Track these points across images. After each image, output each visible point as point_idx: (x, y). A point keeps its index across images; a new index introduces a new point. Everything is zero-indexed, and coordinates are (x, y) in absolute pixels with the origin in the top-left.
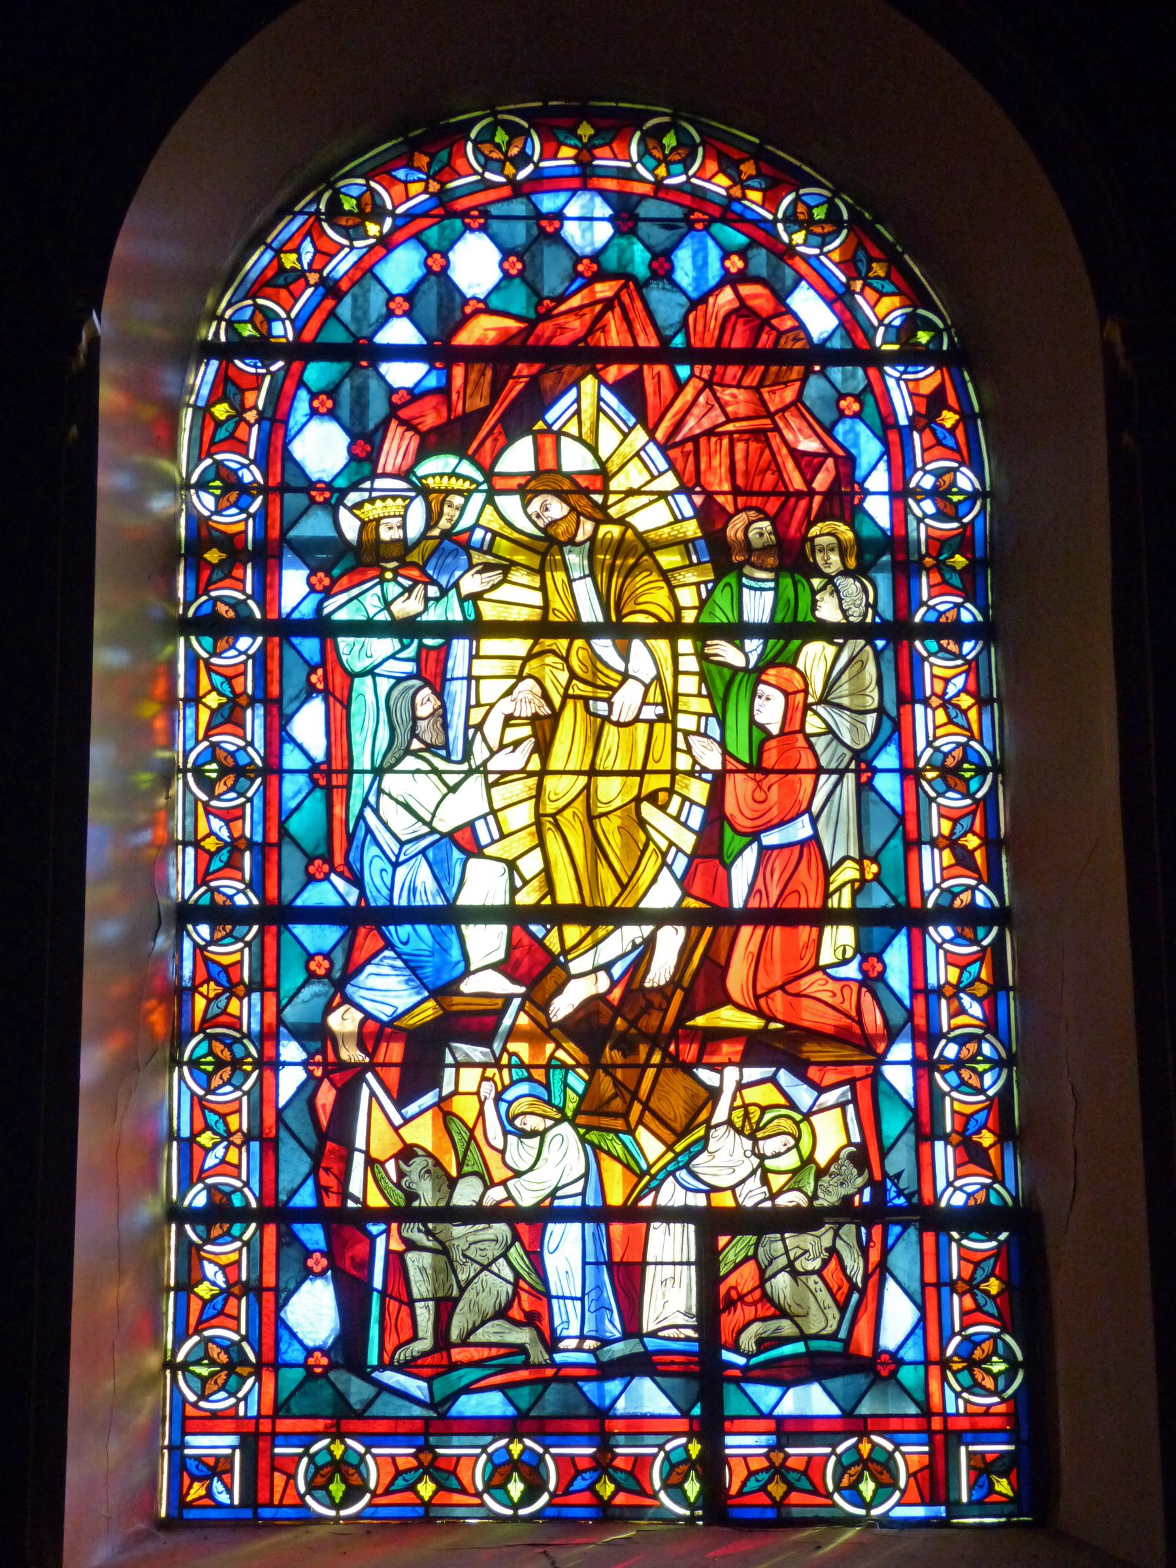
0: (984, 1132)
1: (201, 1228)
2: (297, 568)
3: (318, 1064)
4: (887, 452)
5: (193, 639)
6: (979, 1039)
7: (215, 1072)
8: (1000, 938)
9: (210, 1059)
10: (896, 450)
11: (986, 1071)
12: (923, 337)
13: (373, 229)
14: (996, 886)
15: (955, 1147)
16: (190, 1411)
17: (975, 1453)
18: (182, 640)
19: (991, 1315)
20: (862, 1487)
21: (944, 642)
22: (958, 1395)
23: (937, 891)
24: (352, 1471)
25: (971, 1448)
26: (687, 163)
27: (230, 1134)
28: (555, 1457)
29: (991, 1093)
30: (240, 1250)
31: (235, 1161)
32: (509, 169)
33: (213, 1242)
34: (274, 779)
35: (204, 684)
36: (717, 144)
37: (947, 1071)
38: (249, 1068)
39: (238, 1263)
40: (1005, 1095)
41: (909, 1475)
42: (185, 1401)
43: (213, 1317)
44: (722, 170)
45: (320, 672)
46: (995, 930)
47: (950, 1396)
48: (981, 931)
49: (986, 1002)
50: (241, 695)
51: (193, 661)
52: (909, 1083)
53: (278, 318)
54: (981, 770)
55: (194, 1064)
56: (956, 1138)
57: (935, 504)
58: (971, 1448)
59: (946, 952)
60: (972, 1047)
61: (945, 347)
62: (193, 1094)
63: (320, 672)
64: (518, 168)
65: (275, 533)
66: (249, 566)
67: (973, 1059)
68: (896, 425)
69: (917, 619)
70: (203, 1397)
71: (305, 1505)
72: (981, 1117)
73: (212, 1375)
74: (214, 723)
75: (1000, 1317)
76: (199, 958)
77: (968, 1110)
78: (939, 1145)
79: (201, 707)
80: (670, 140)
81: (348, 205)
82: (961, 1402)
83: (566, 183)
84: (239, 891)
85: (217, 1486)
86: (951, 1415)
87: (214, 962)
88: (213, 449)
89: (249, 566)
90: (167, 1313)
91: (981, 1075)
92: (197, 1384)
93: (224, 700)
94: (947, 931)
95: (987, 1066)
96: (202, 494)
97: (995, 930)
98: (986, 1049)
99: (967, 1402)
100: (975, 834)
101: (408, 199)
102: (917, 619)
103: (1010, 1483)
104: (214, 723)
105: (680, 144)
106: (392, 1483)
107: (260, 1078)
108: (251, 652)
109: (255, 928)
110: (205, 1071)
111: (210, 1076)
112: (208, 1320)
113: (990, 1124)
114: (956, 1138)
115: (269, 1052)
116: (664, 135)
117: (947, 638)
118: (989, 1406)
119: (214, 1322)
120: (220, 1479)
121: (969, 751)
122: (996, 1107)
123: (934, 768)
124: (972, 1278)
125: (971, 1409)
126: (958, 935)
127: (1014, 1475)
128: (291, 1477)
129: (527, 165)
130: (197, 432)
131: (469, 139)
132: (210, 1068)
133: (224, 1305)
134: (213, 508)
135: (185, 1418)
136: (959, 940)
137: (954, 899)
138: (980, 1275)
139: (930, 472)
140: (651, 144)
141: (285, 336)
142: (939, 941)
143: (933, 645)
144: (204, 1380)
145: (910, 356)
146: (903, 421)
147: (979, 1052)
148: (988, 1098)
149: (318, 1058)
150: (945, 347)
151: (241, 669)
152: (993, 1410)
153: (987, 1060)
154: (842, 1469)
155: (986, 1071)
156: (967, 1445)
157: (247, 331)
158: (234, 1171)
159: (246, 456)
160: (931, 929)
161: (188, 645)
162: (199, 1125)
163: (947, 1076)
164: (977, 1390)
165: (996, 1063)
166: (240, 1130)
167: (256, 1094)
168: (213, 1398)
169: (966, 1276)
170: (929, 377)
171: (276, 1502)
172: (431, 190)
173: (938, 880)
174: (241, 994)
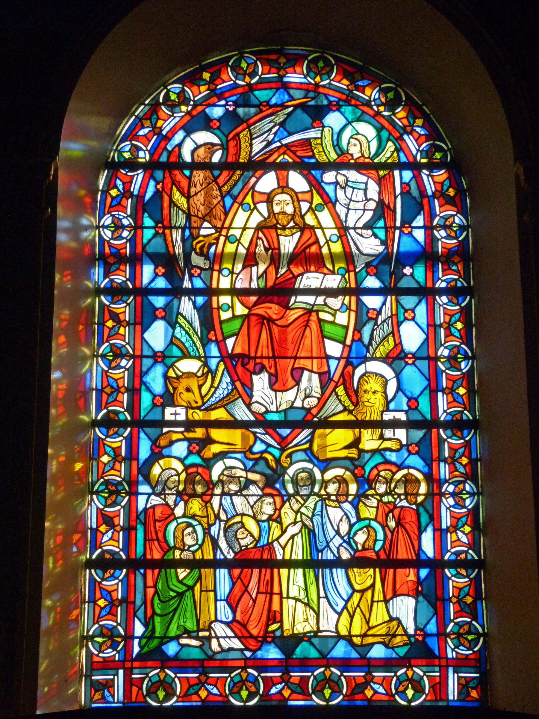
0: (466, 526)
1: (104, 430)
2: (149, 264)
3: (160, 228)
4: (436, 614)
5: (97, 429)
6: (464, 482)
7: (113, 360)
8: (479, 574)
9: (111, 354)
10: (440, 610)
11: (467, 498)
12: (438, 156)
13: (184, 108)
14: (472, 411)
15: (449, 464)
16: (96, 659)
17: (462, 677)
18: (88, 571)
19: (457, 337)
20: (407, 692)
21: (459, 570)
22: (453, 650)
23: (445, 414)
24: (168, 686)
25: (460, 675)
26: (329, 74)
27: (119, 388)
28: (119, 510)
29: (464, 371)
30: (125, 307)
31: (123, 333)
32: (247, 79)
33: (110, 437)
34: (139, 231)
35: (98, 595)
36: (344, 66)
37: (449, 497)
38: (124, 495)
39: (120, 447)
40: (476, 508)
41: (430, 687)
42: (92, 654)
43: (114, 335)
44: (345, 77)
45: (161, 184)
46: (476, 571)
47: (449, 651)
48: (465, 432)
49: (469, 536)
50: (116, 600)
51: (92, 580)
52: (423, 237)
53: (141, 149)
54: (466, 357)
55: (103, 356)
56: (449, 461)
57: (446, 232)
58: (460, 675)
59: (451, 511)
60: (461, 486)
61: (449, 160)
62: (98, 508)
63: (161, 184)
64: (252, 78)
65: (139, 249)
66: (128, 265)
67: (461, 493)
68: (427, 196)
69: (446, 558)
70: (100, 651)
71: (146, 702)
72: (466, 589)
73: (104, 642)
74: (111, 334)
75: (461, 338)
76: (99, 514)
77: (461, 586)
78: (442, 464)
79: (104, 394)
80: (321, 64)
81: (173, 97)
82: (454, 653)
83: (273, 85)
84: (124, 217)
85: (107, 693)
86: (450, 659)
87: (111, 377)
88: (111, 209)
89: (128, 265)
90: (92, 398)
91: (464, 500)
92: (97, 646)
93: (111, 458)
94: (444, 299)
95: (468, 496)
96: (105, 230)
97: (476, 571)
98: (468, 488)
99: (457, 653)
100: (470, 596)
101: (200, 93)
102: (446, 558)
103: (477, 692)
104: (111, 334)
105: (325, 65)
106: (187, 691)
107: (129, 500)
108: (127, 367)
109: (132, 298)
110: (108, 359)
111: (111, 361)
112: (103, 617)
113: (469, 522)
114: (449, 461)
115: (134, 489)
116: (318, 62)
117: (461, 568)
118: (468, 655)
119: (109, 473)
120: (108, 691)
121: (460, 349)
122: (466, 376)
123: (454, 633)
124: (453, 387)
125: (459, 656)
126: (450, 301)
127: (479, 689)
128: (141, 688)
129: (256, 76)
130: (108, 179)
131: (228, 65)
132: (111, 358)
133: (117, 396)
134: (110, 237)
135: (92, 662)
136: (456, 506)
137: (460, 628)
138: (455, 386)
139: (445, 281)
140: (312, 66)
141: (145, 158)
142: (448, 506)
143: (453, 571)
144: (101, 645)
145: (432, 166)
146: (430, 193)
147: (464, 489)
148: (463, 373)
149: (160, 225)
150: (449, 160)
151: (115, 587)
152: (470, 657)
153: (468, 493)
154: (399, 682)
155: (467, 498)
156: (458, 673)
157: (127, 155)
158: (122, 338)
159: (126, 213)
160: (437, 297)
161: (90, 573)
162: (105, 384)
163: (448, 500)
164: (458, 576)
165: (472, 495)
166: (124, 386)
167: (127, 507)
168: (105, 652)
169: (450, 386)
170: (441, 175)
171: (133, 700)
172: (205, 678)
173: (446, 409)
174: (125, 325)
